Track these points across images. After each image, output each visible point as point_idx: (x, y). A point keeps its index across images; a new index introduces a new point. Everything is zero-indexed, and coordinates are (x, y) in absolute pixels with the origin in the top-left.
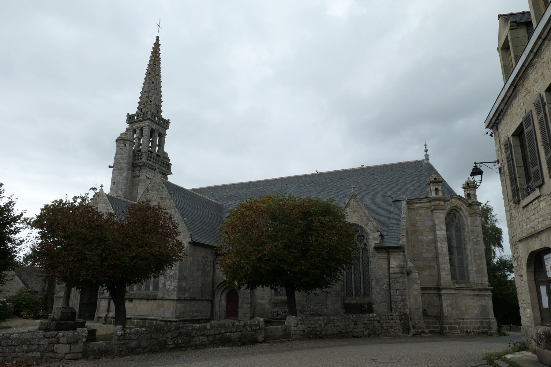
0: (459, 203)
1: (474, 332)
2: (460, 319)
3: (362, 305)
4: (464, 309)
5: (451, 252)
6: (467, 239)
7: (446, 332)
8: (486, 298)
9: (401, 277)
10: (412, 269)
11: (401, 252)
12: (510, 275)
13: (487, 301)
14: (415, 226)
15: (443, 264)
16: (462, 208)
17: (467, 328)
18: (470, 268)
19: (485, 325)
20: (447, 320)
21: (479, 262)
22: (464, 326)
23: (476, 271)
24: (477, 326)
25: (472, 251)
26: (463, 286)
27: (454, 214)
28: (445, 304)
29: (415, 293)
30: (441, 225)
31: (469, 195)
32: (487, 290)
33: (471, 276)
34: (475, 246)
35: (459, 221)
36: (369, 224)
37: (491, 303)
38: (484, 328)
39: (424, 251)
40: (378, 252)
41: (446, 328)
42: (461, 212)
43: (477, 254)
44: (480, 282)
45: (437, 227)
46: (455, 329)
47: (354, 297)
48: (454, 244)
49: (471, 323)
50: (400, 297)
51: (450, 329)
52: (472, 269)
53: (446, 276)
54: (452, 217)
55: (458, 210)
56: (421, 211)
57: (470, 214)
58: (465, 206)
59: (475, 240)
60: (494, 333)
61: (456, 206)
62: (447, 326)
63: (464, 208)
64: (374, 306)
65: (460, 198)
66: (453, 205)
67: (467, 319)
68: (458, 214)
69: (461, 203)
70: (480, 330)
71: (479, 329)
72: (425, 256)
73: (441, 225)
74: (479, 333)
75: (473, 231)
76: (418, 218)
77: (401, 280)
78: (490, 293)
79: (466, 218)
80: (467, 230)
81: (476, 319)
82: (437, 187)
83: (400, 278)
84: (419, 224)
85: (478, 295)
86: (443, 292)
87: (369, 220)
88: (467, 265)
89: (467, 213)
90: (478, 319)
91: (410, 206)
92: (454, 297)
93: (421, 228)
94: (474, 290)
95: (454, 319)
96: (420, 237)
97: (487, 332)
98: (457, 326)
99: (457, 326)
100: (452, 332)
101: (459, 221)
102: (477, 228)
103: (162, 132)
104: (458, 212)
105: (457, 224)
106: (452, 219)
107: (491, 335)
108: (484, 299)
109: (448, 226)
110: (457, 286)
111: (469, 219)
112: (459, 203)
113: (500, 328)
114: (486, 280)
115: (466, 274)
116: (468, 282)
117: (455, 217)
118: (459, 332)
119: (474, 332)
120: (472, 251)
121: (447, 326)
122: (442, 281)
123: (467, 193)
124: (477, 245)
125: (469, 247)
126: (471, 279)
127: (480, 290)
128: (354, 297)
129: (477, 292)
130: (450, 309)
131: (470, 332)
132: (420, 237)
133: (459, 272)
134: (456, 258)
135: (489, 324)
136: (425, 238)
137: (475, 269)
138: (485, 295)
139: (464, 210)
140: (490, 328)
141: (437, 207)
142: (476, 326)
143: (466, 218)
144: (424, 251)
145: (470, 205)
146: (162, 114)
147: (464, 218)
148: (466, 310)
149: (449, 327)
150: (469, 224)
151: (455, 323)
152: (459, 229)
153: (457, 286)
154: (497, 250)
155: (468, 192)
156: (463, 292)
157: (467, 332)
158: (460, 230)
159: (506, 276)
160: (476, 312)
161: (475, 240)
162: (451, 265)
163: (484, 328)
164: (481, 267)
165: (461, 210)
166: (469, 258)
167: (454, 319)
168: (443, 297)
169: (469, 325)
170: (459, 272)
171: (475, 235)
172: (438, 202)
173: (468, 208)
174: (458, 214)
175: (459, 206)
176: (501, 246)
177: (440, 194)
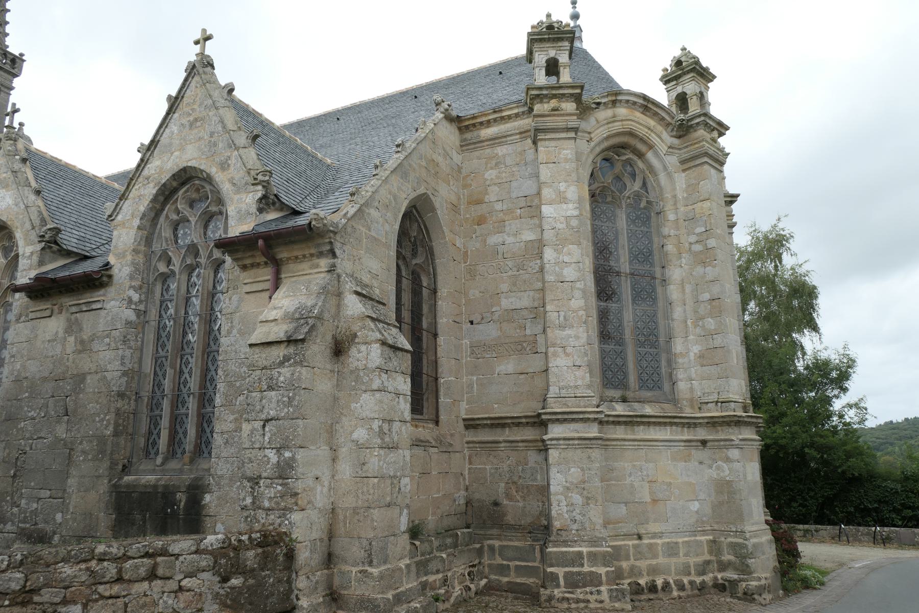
0: (642, 123)
1: (681, 587)
2: (627, 536)
3: (167, 495)
4: (648, 499)
5: (605, 288)
6: (670, 248)
7: (550, 598)
8: (734, 453)
9: (286, 359)
10: (355, 328)
11: (321, 255)
12: (837, 397)
13: (736, 465)
14: (479, 202)
15: (562, 327)
16: (654, 139)
17: (653, 570)
18: (678, 346)
19: (727, 557)
20: (565, 543)
21: (711, 323)
22: (643, 564)
23: (701, 356)
24: (700, 559)
25: (688, 288)
26: (648, 410)
27: (629, 162)
28: (557, 481)
29: (360, 434)
30: (562, 186)
31: (682, 101)
32: (737, 422)
33: (680, 375)
34: (699, 270)
35: (644, 184)
36: (232, 162)
37: (751, 472)
38: (723, 567)
39: (504, 287)
40: (244, 268)
41: (554, 577)
42: (650, 155)
43: (706, 296)
44: (714, 397)
45: (546, 192)
46: (594, 580)
47: (159, 460)
48: (623, 262)
49: (672, 550)
50: (272, 456)
51: (573, 582)
52: (687, 348)
53: (571, 368)
54: (617, 172)
55: (641, 147)
56: (501, 151)
57: (683, 162)
58: (665, 135)
59: (698, 248)
60: (761, 590)
61: (631, 134)
62: (560, 571)
63: (662, 139)
64: (207, 498)
65: (647, 104)
66: (617, 127)
67: (655, 535)
68: (640, 164)
69: (652, 123)
70: (708, 578)
71: (703, 573)
72: (505, 303)
73: (562, 186)
74: (702, 587)
75: (691, 219)
76: (491, 174)
77: (285, 372)
78: (749, 434)
79: (669, 175)
80: (671, 217)
81: (694, 533)
82: (552, 53)
83: (281, 364)
84: (493, 194)
85: (704, 443)
86: (556, 431)
87: (233, 146)
88: (670, 339)
89: (672, 161)
90: (704, 532)
91: (468, 135)
92: (596, 454)
93: (498, 206)
94: (691, 424)
95: (594, 542)
96: (493, 240)
97: (734, 583)
98: (602, 570)
99: (602, 570)
100: (579, 594)
101: (644, 184)
102: (707, 204)
103: (7, 83)
104: (641, 155)
105: (637, 196)
106: (618, 178)
107: (748, 597)
108: (728, 460)
109: (600, 197)
110: (620, 409)
111: (681, 180)
112: (642, 123)
113: (787, 554)
114: (737, 388)
115: (664, 370)
116: (674, 401)
117: (633, 176)
118: (605, 596)
119: (681, 587)
120: (688, 288)
121: (560, 571)
122: (553, 391)
123: (674, 94)
124: (704, 263)
125: (676, 274)
126: (682, 386)
127: (714, 423)
128: (159, 460)
129: (702, 434)
130: (577, 499)
131: (666, 585)
132: (493, 240)
133: (632, 359)
134: (628, 314)
135: (743, 556)
136: (510, 240)
137: (696, 349)
138: (728, 444)
139: (662, 148)
140: (745, 570)
141: (551, 122)
142: (693, 560)
143: (669, 175)
144: (504, 287)
145: (683, 130)
146: (8, 41)
147: (662, 177)
148: (655, 501)
149: (566, 575)
150: (680, 195)
151: (593, 557)
152: (646, 213)
153: (620, 409)
154: (807, 340)
155: (679, 89)
156: (642, 433)
157: (653, 588)
158: (649, 218)
159: (828, 401)
160: (695, 506)
161: (698, 248)
162: (604, 336)
163: (723, 567)
164: (718, 341)
165: (651, 147)
166: (678, 312)
167: (594, 542)
168: (553, 454)
169: (661, 560)
170: (632, 359)
171: (700, 230)
172: (554, 103)
173: (676, 141)
174: (640, 164)
175: (642, 131)
176: (815, 328)
177: (565, 77)
